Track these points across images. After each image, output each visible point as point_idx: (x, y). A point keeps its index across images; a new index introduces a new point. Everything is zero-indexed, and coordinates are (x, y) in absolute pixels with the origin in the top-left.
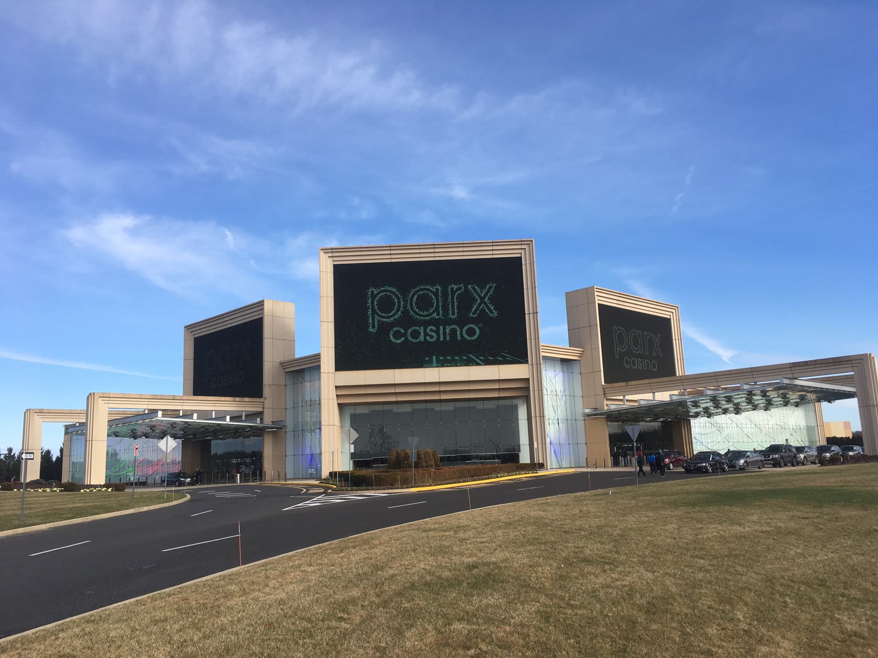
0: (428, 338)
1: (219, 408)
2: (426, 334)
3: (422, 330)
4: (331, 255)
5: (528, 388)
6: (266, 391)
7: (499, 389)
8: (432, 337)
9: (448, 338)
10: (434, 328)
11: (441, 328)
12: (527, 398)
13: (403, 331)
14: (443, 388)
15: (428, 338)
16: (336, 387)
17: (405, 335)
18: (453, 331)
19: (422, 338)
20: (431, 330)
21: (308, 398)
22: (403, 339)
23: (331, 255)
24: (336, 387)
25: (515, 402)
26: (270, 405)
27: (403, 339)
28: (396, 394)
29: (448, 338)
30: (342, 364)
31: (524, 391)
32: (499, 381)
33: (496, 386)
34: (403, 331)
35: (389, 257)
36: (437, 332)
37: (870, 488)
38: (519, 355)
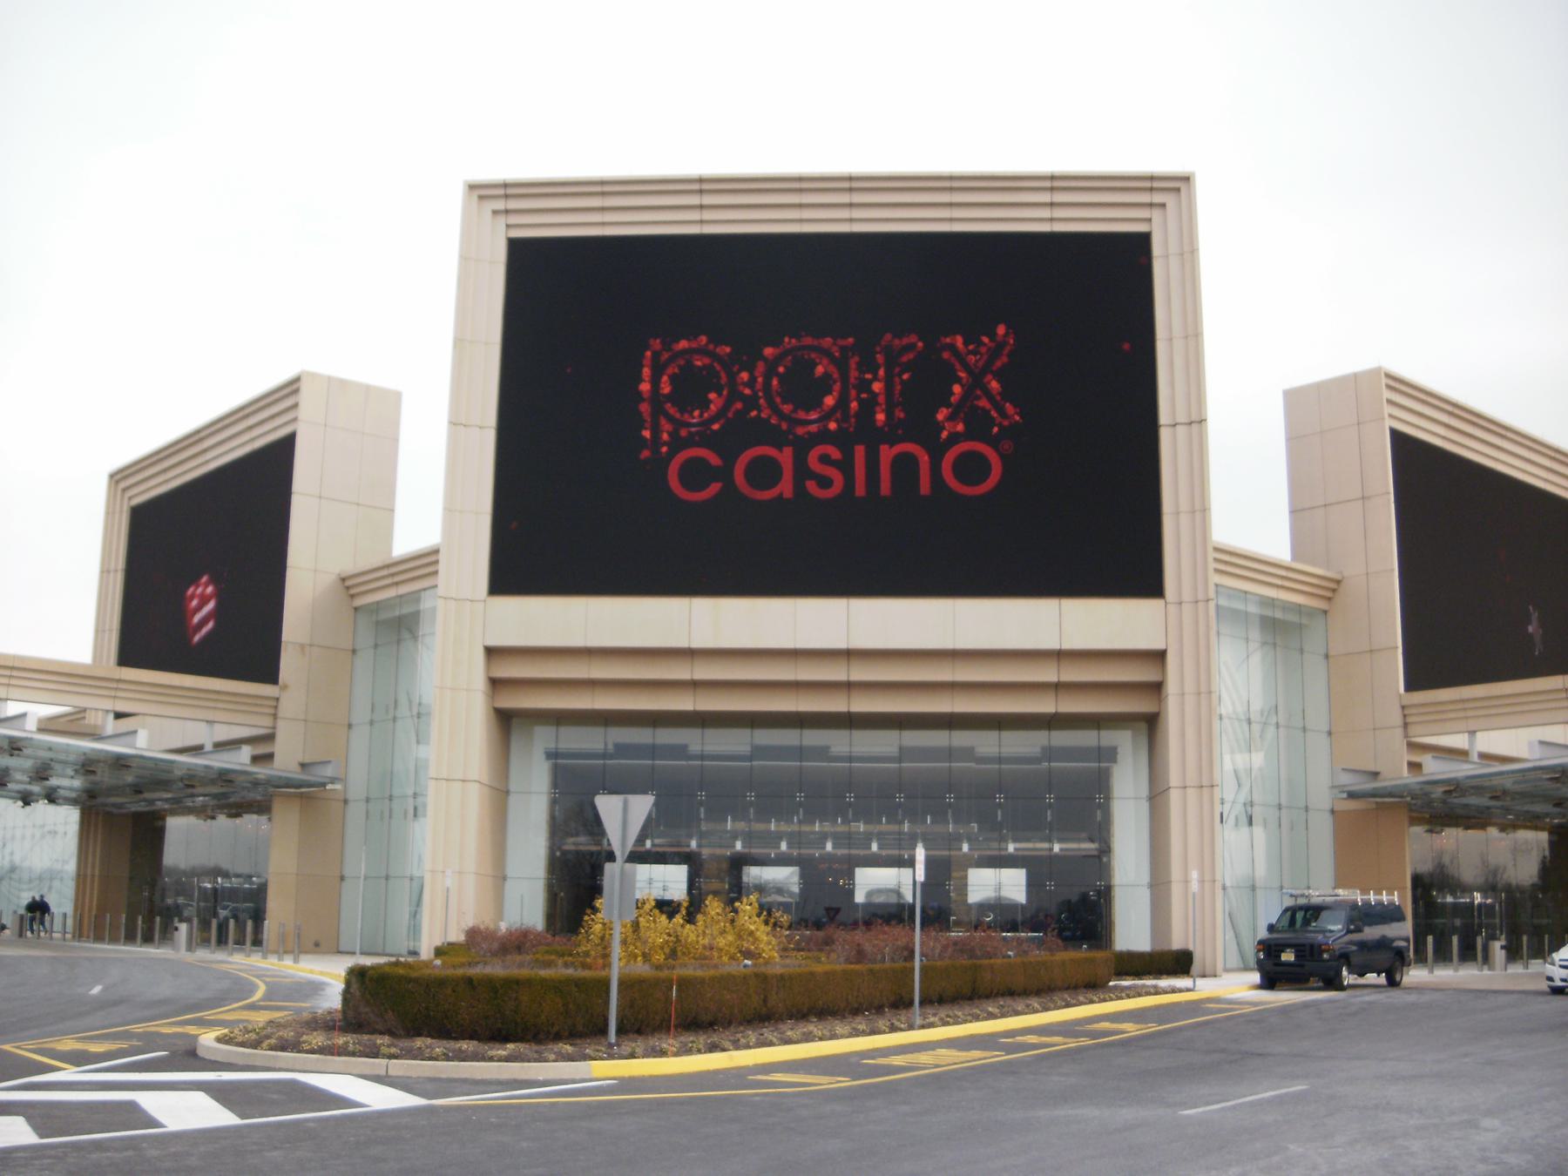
0: (811, 486)
1: (172, 722)
2: (802, 472)
3: (785, 457)
4: (500, 205)
5: (1157, 688)
6: (289, 663)
7: (1058, 687)
8: (825, 482)
9: (885, 488)
10: (835, 454)
11: (860, 451)
12: (1151, 723)
13: (715, 460)
14: (860, 673)
15: (811, 486)
16: (491, 652)
17: (725, 474)
18: (904, 465)
19: (785, 487)
20: (825, 460)
21: (1258, 830)
22: (715, 488)
23: (500, 205)
24: (491, 652)
25: (1109, 737)
26: (292, 714)
27: (715, 488)
28: (695, 685)
29: (885, 488)
30: (519, 565)
31: (1137, 701)
32: (1060, 656)
33: (1048, 674)
34: (715, 460)
35: (695, 216)
36: (846, 466)
37: (1320, 937)
38: (1134, 568)
